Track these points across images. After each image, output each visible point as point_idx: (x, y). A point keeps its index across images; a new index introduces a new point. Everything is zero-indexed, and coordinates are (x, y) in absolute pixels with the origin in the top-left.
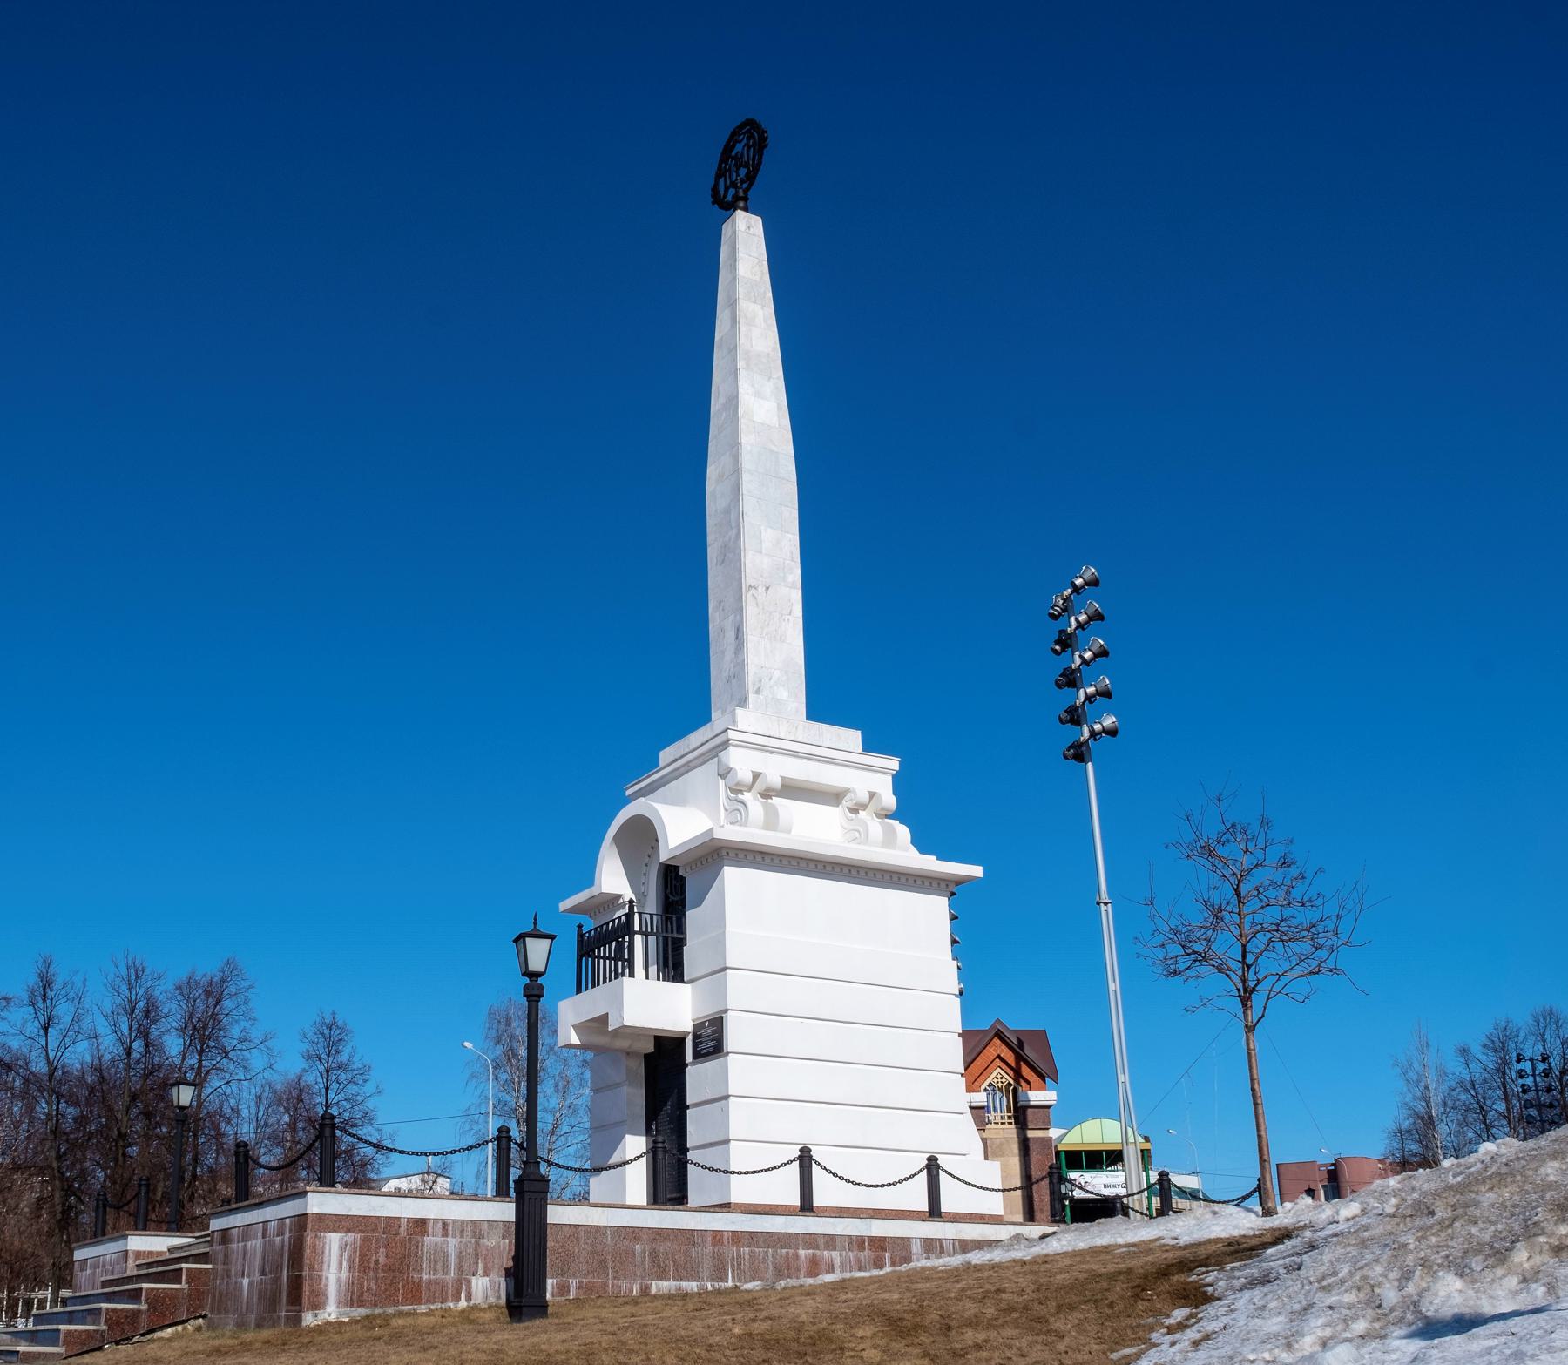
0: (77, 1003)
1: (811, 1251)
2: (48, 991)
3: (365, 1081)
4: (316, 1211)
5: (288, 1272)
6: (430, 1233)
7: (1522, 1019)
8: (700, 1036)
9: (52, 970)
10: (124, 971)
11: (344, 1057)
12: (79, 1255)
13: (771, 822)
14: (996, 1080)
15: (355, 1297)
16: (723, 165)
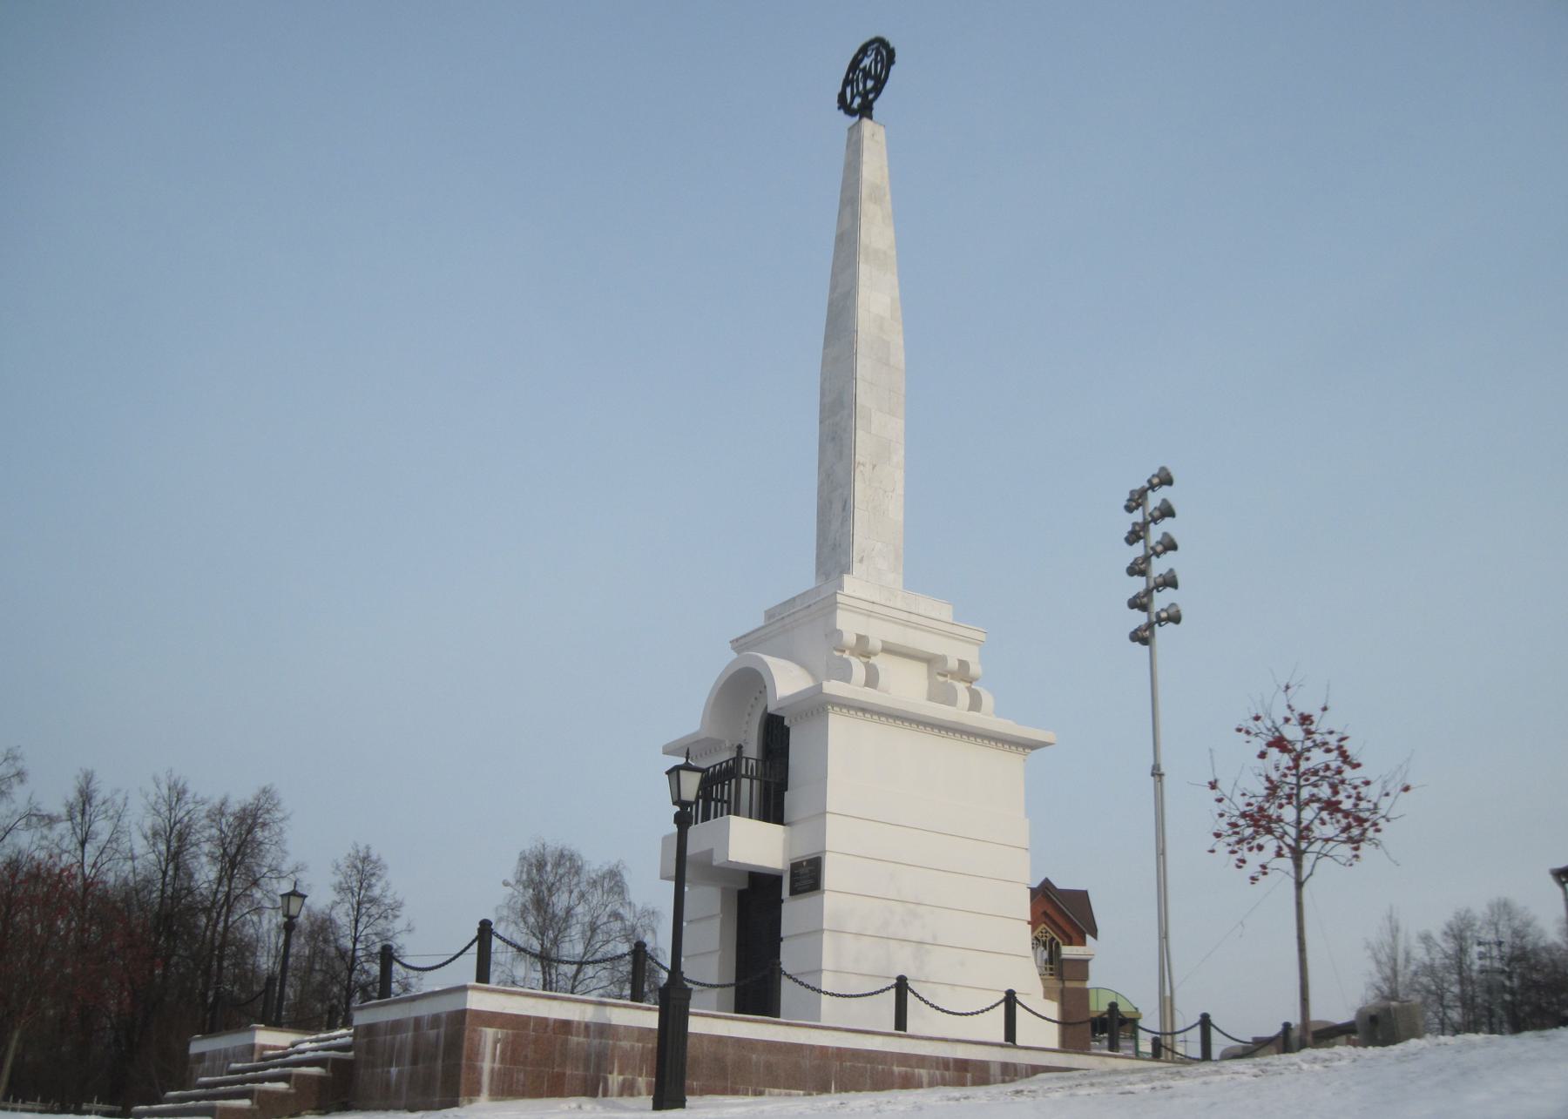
0: (116, 820)
1: (904, 1069)
2: (87, 807)
3: (396, 917)
4: (474, 1007)
5: (443, 1061)
6: (574, 1033)
7: (1480, 910)
8: (798, 875)
9: (93, 786)
10: (165, 791)
11: (376, 892)
12: (198, 1046)
13: (872, 680)
14: (1040, 934)
15: (506, 1086)
16: (851, 75)
